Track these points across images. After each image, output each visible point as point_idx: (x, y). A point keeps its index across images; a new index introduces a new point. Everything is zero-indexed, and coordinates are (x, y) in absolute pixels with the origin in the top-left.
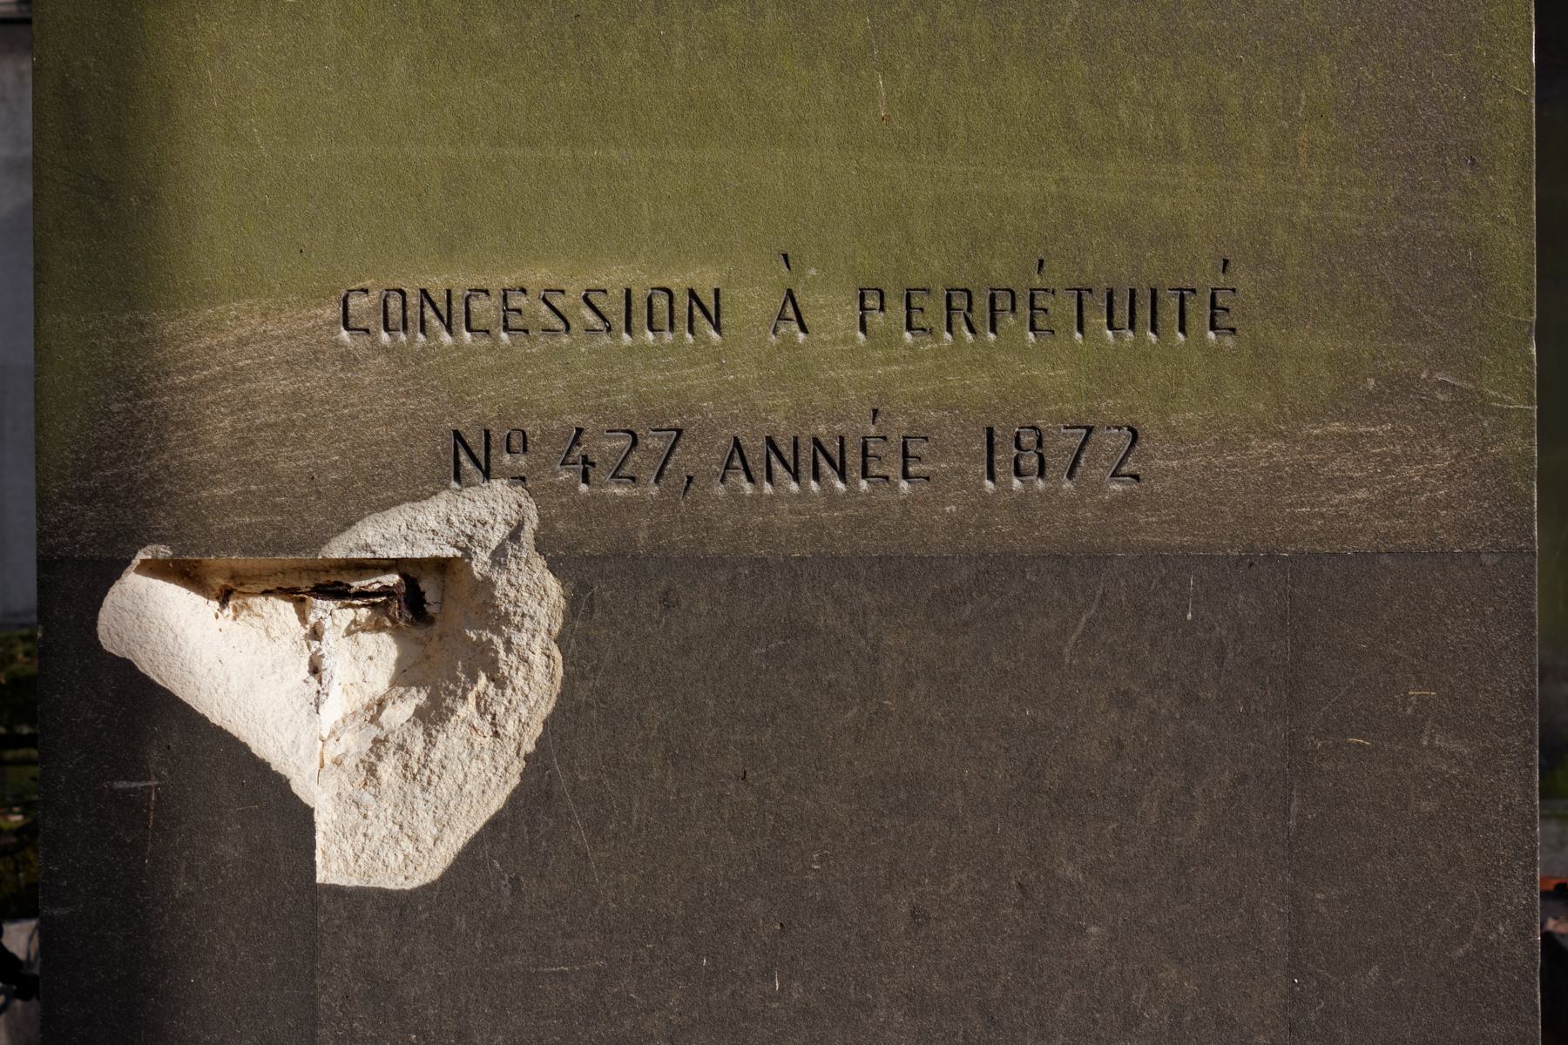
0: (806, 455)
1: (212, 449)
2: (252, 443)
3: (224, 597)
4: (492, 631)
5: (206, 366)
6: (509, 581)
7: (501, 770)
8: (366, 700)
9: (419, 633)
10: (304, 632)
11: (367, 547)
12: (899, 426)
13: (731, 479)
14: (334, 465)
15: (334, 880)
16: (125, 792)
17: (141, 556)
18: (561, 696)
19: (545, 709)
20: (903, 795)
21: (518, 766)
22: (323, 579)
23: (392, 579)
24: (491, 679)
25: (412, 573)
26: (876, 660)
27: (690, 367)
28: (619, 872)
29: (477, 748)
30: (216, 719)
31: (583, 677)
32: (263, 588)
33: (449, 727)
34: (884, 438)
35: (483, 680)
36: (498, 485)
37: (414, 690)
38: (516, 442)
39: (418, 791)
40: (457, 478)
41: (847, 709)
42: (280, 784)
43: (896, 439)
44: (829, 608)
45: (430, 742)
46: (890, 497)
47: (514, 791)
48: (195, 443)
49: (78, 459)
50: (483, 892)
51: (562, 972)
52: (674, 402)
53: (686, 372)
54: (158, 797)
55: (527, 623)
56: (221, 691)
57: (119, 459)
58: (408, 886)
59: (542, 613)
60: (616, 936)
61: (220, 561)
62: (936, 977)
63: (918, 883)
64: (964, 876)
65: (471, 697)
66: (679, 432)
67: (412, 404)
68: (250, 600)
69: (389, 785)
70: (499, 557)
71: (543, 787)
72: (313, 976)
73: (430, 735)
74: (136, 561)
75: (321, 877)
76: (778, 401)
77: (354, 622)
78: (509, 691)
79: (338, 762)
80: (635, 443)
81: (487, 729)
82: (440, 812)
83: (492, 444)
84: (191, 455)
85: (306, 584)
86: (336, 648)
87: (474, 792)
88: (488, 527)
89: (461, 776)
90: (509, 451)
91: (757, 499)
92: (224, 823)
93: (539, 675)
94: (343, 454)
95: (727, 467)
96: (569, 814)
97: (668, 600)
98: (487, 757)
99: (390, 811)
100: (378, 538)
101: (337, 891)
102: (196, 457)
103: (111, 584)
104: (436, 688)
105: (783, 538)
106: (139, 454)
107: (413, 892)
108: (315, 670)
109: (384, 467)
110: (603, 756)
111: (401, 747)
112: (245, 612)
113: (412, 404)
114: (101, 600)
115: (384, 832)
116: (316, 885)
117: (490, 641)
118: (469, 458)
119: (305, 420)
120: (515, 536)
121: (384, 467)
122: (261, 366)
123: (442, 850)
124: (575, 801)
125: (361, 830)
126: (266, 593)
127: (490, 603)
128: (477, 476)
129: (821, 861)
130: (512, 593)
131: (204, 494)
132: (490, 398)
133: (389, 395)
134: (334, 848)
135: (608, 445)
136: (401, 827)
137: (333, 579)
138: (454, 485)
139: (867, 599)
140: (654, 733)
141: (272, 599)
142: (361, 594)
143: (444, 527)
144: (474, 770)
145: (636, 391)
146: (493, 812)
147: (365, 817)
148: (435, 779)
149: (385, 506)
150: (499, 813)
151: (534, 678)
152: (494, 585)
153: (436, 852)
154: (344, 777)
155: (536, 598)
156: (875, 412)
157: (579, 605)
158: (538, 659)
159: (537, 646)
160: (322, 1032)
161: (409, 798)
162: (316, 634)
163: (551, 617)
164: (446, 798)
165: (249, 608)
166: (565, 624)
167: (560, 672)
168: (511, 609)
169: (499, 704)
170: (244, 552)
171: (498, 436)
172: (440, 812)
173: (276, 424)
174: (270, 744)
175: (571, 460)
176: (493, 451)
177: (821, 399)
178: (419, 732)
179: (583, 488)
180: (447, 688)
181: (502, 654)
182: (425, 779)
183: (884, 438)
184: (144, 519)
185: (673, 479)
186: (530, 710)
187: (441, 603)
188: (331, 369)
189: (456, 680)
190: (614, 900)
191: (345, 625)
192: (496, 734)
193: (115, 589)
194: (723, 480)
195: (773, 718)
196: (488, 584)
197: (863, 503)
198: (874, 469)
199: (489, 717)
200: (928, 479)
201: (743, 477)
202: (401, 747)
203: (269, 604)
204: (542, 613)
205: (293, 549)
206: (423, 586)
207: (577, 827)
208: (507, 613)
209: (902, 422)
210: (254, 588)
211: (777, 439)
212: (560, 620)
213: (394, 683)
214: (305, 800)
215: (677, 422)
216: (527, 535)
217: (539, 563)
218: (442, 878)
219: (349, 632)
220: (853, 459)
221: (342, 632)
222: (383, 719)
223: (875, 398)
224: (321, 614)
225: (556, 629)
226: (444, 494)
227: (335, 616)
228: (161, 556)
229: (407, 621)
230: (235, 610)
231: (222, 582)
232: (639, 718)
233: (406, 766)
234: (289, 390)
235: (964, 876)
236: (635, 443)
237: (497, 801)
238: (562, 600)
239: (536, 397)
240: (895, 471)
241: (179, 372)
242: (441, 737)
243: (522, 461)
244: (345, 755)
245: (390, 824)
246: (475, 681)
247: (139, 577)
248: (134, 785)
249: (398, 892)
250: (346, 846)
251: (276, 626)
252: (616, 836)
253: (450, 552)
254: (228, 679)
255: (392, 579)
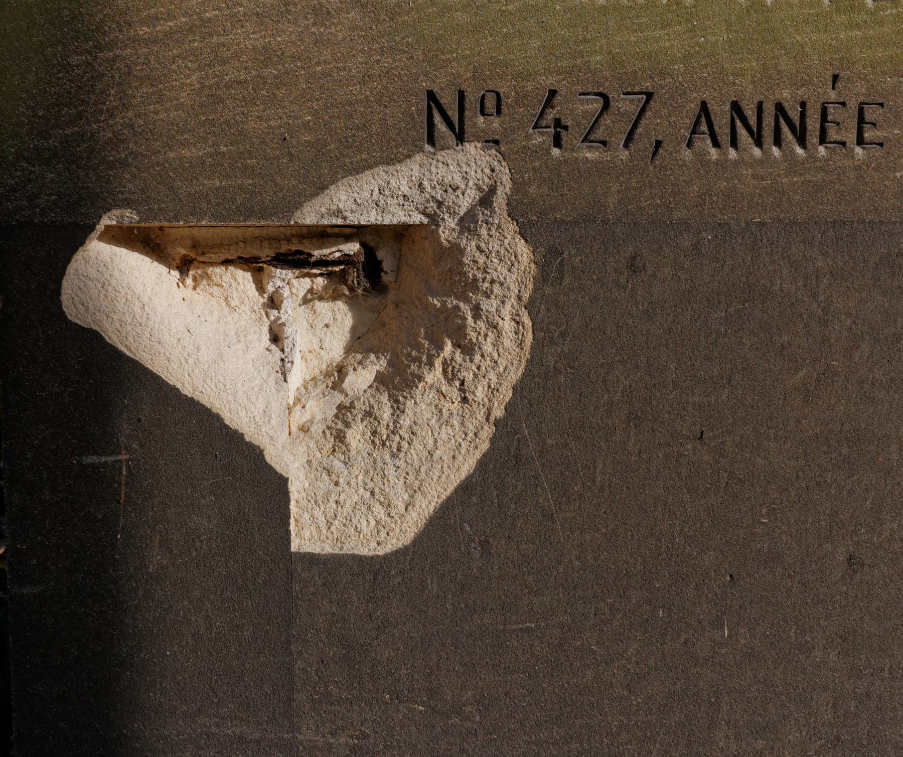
0: (769, 120)
1: (179, 106)
2: (221, 101)
3: (184, 266)
4: (457, 298)
5: (171, 16)
6: (478, 247)
7: (471, 435)
8: (324, 367)
9: (375, 301)
10: (262, 301)
11: (338, 212)
12: (856, 92)
13: (697, 144)
14: (306, 125)
15: (308, 548)
16: (94, 467)
17: (106, 221)
18: (530, 361)
19: (515, 375)
20: (845, 451)
21: (488, 431)
22: (284, 248)
23: (352, 248)
24: (457, 345)
25: (369, 239)
26: (826, 322)
27: (661, 29)
28: (583, 531)
29: (445, 413)
30: (187, 391)
31: (552, 342)
32: (223, 257)
33: (418, 393)
34: (843, 104)
35: (448, 347)
36: (472, 149)
37: (372, 357)
38: (490, 104)
39: (387, 457)
40: (431, 140)
41: (797, 369)
42: (253, 454)
43: (853, 104)
44: (785, 272)
45: (398, 409)
46: (847, 163)
47: (484, 455)
48: (160, 100)
49: (35, 116)
50: (454, 555)
51: (528, 628)
52: (646, 64)
53: (658, 33)
54: (129, 471)
55: (497, 289)
56: (191, 361)
57: (80, 116)
58: (381, 551)
59: (512, 280)
60: (579, 593)
61: (180, 229)
62: (867, 618)
63: (855, 532)
64: (895, 525)
65: (438, 363)
66: (649, 95)
67: (386, 62)
68: (210, 270)
69: (358, 452)
70: (468, 223)
71: (513, 450)
72: (289, 643)
73: (397, 401)
74: (100, 227)
75: (295, 546)
76: (745, 65)
77: (311, 291)
78: (477, 358)
79: (304, 429)
80: (606, 105)
81: (455, 394)
82: (411, 478)
83: (467, 105)
84: (156, 113)
85: (267, 253)
86: (292, 312)
87: (445, 458)
88: (459, 192)
89: (431, 442)
90: (483, 113)
91: (722, 164)
92: (197, 495)
93: (508, 341)
94: (315, 113)
95: (694, 132)
96: (536, 477)
97: (634, 266)
98: (456, 422)
99: (360, 478)
100: (350, 203)
101: (312, 559)
102: (163, 115)
103: (74, 250)
104: (395, 355)
105: (745, 204)
106: (101, 112)
107: (386, 557)
108: (276, 339)
109: (357, 128)
110: (570, 420)
111: (369, 414)
112: (204, 282)
113: (386, 62)
114: (64, 269)
115: (356, 498)
116: (291, 554)
117: (457, 308)
118: (443, 120)
119: (276, 77)
120: (486, 200)
121: (357, 128)
122: (229, 17)
123: (414, 515)
124: (542, 465)
125: (333, 497)
126: (226, 262)
127: (458, 269)
128: (451, 140)
129: (768, 515)
130: (481, 260)
131: (172, 155)
132: (465, 57)
133: (362, 51)
134: (306, 516)
135: (580, 108)
136: (372, 493)
137: (294, 248)
138: (428, 148)
139: (820, 264)
140: (618, 396)
141: (231, 268)
142: (322, 263)
143: (414, 193)
144: (444, 436)
145: (610, 52)
146: (463, 477)
147: (337, 484)
148: (405, 445)
149: (357, 169)
150: (469, 478)
151: (503, 347)
152: (462, 251)
153: (408, 518)
154: (312, 444)
155: (507, 263)
156: (835, 78)
157: (549, 267)
158: (507, 325)
159: (506, 312)
160: (300, 697)
161: (380, 464)
162: (274, 303)
163: (521, 283)
164: (417, 464)
165: (209, 277)
166: (535, 290)
167: (529, 338)
168: (480, 276)
169: (467, 369)
170: (214, 217)
171: (472, 98)
172: (411, 478)
173: (246, 81)
174: (243, 414)
175: (544, 123)
176: (467, 113)
177: (786, 64)
178: (384, 398)
179: (556, 152)
180: (409, 355)
181: (470, 321)
182: (395, 445)
183: (843, 104)
184: (108, 182)
185: (643, 144)
186: (499, 376)
187: (398, 271)
188: (303, 22)
189: (418, 347)
190: (578, 558)
191: (302, 294)
192: (465, 400)
193: (79, 256)
194: (690, 145)
195: (729, 381)
196: (456, 250)
197: (821, 168)
198: (833, 134)
199: (457, 383)
200: (881, 145)
201: (709, 142)
202: (369, 414)
203: (229, 274)
204: (512, 280)
205: (264, 213)
206: (381, 255)
207: (543, 489)
208: (475, 280)
209: (861, 87)
210: (214, 257)
211: (743, 104)
212: (531, 286)
213: (349, 350)
214: (279, 469)
215: (648, 85)
216: (500, 200)
217: (511, 228)
218: (414, 543)
219: (305, 301)
220: (813, 124)
221: (300, 300)
222: (346, 385)
223: (836, 63)
224: (279, 283)
225: (526, 296)
226: (418, 158)
227: (293, 285)
228: (126, 221)
229: (364, 290)
230: (195, 279)
231: (183, 251)
232: (604, 382)
233: (374, 433)
234: (259, 44)
235: (895, 525)
236: (606, 105)
237: (467, 466)
238: (533, 266)
239: (512, 56)
240: (851, 137)
241: (144, 22)
242: (410, 403)
243: (496, 123)
244: (311, 421)
245: (361, 491)
246: (440, 348)
247: (102, 244)
248: (104, 459)
249: (372, 557)
250: (318, 513)
251: (235, 295)
252: (581, 496)
253: (417, 218)
254: (198, 349)
255: (352, 248)
